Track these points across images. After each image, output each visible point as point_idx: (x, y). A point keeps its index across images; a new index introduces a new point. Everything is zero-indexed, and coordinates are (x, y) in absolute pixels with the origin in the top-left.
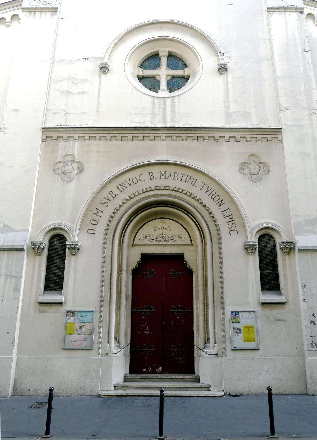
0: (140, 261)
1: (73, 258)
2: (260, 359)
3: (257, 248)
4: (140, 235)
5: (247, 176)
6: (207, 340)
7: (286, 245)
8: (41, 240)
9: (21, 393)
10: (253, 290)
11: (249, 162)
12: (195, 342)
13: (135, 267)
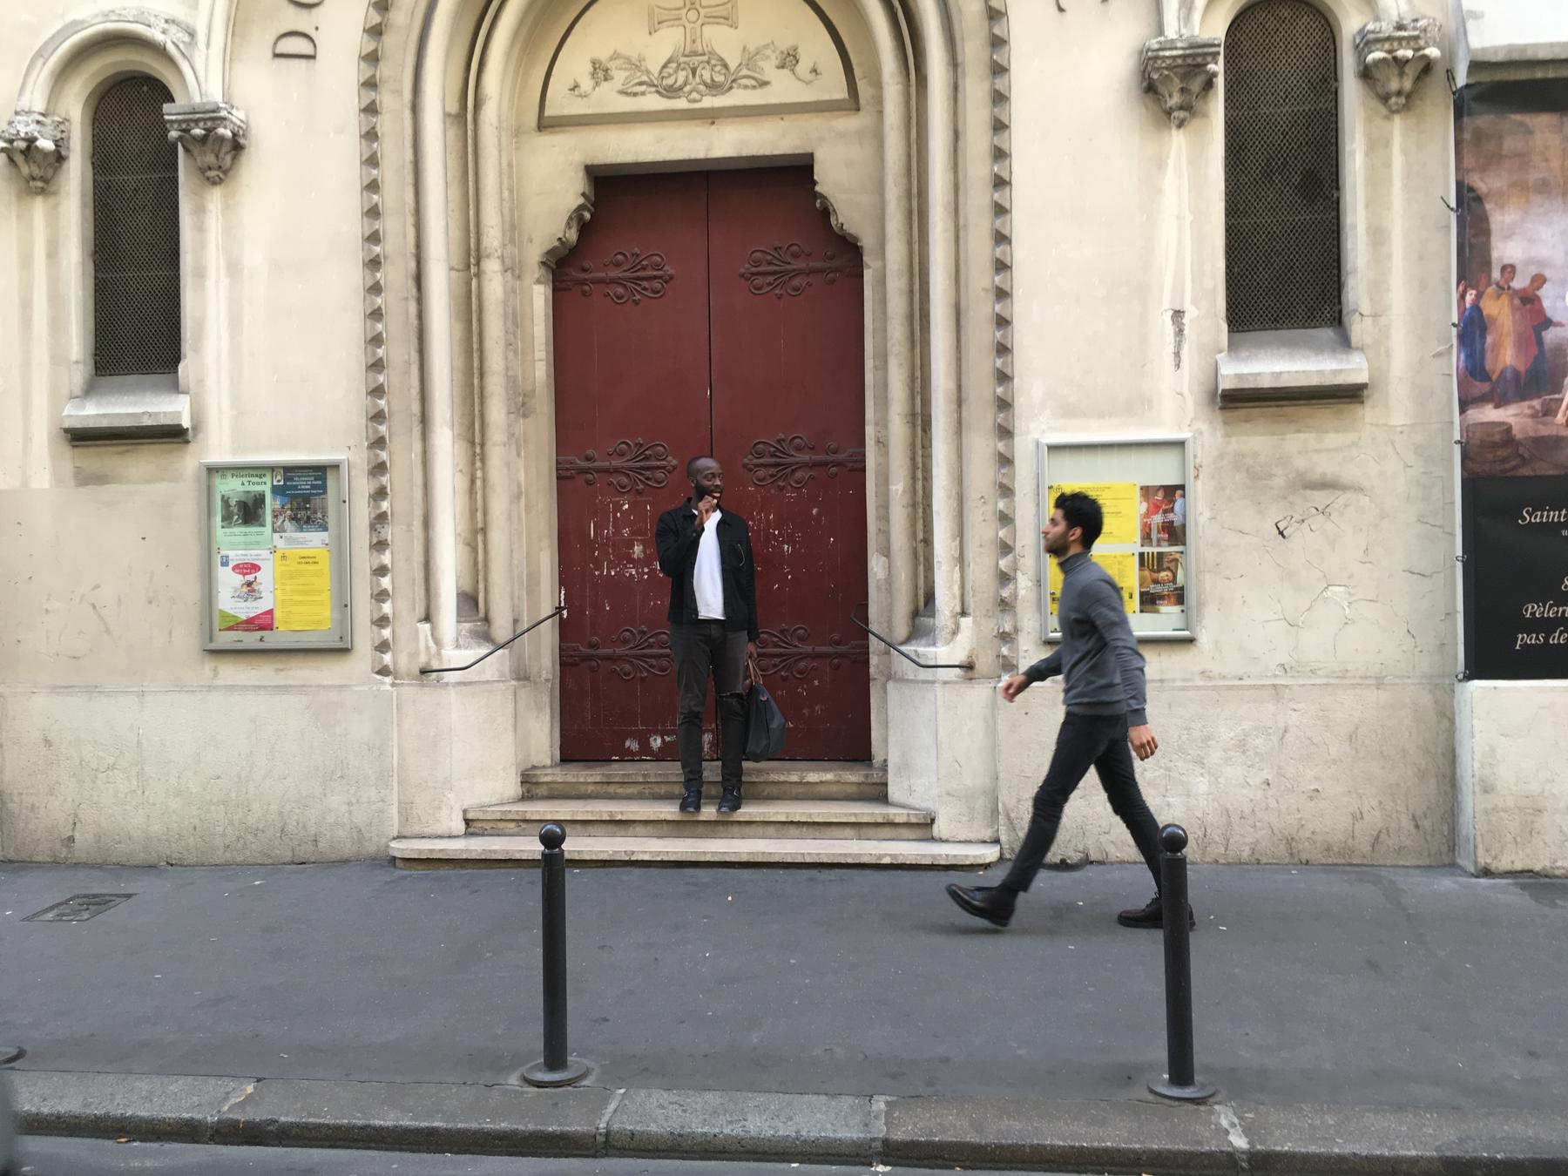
0: (581, 208)
1: (215, 197)
3: (1220, 82)
4: (574, 65)
6: (924, 603)
12: (873, 611)
13: (556, 243)
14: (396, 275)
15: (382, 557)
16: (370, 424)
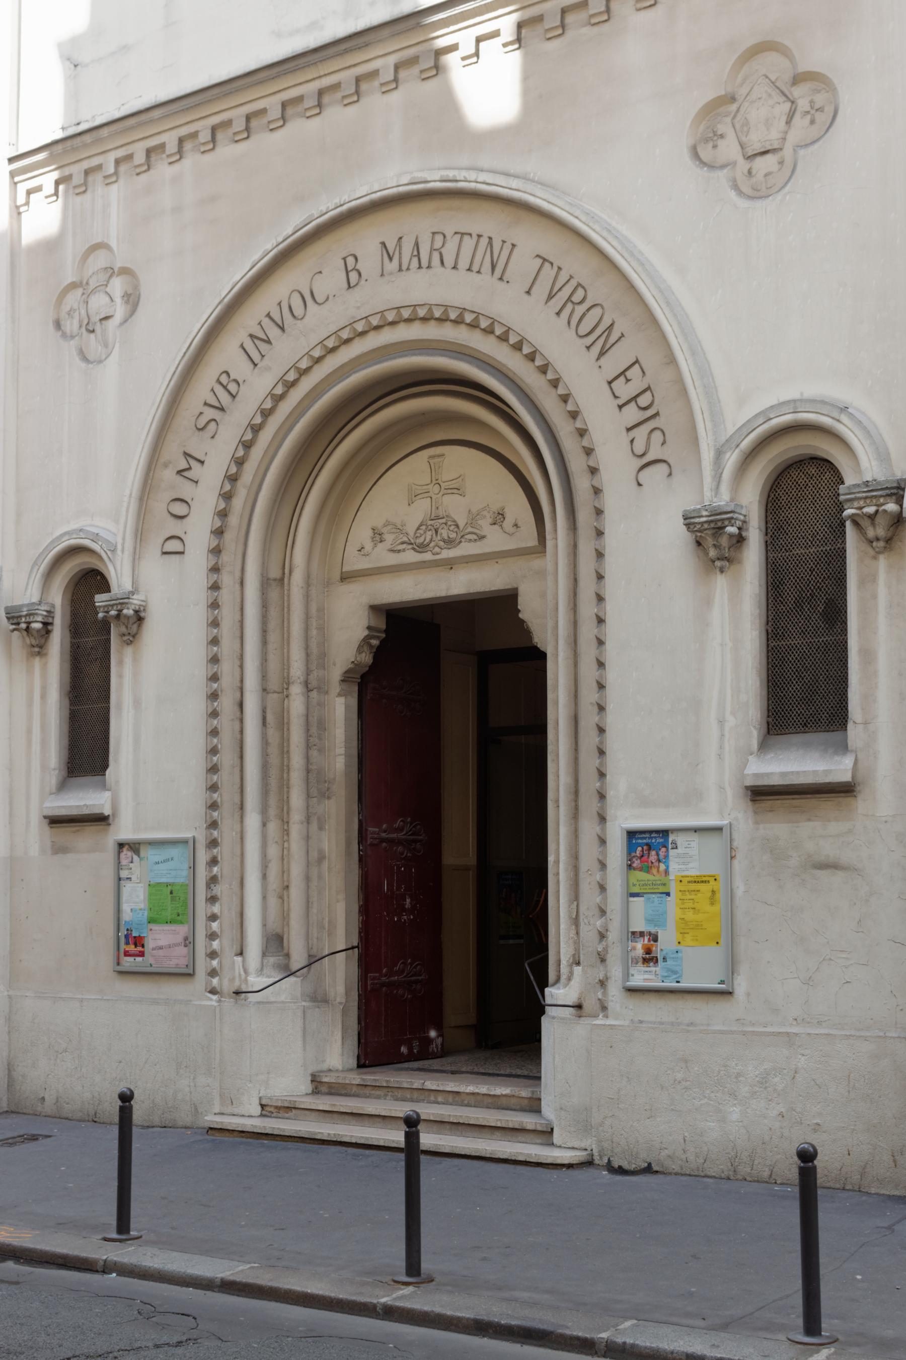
1: (129, 651)
2: (732, 1032)
4: (361, 533)
5: (723, 174)
7: (862, 503)
8: (35, 599)
9: (25, 1108)
10: (723, 735)
11: (743, 91)
13: (352, 666)
14: (227, 703)
15: (213, 907)
16: (208, 810)
